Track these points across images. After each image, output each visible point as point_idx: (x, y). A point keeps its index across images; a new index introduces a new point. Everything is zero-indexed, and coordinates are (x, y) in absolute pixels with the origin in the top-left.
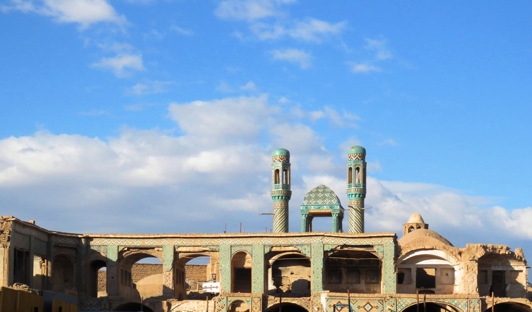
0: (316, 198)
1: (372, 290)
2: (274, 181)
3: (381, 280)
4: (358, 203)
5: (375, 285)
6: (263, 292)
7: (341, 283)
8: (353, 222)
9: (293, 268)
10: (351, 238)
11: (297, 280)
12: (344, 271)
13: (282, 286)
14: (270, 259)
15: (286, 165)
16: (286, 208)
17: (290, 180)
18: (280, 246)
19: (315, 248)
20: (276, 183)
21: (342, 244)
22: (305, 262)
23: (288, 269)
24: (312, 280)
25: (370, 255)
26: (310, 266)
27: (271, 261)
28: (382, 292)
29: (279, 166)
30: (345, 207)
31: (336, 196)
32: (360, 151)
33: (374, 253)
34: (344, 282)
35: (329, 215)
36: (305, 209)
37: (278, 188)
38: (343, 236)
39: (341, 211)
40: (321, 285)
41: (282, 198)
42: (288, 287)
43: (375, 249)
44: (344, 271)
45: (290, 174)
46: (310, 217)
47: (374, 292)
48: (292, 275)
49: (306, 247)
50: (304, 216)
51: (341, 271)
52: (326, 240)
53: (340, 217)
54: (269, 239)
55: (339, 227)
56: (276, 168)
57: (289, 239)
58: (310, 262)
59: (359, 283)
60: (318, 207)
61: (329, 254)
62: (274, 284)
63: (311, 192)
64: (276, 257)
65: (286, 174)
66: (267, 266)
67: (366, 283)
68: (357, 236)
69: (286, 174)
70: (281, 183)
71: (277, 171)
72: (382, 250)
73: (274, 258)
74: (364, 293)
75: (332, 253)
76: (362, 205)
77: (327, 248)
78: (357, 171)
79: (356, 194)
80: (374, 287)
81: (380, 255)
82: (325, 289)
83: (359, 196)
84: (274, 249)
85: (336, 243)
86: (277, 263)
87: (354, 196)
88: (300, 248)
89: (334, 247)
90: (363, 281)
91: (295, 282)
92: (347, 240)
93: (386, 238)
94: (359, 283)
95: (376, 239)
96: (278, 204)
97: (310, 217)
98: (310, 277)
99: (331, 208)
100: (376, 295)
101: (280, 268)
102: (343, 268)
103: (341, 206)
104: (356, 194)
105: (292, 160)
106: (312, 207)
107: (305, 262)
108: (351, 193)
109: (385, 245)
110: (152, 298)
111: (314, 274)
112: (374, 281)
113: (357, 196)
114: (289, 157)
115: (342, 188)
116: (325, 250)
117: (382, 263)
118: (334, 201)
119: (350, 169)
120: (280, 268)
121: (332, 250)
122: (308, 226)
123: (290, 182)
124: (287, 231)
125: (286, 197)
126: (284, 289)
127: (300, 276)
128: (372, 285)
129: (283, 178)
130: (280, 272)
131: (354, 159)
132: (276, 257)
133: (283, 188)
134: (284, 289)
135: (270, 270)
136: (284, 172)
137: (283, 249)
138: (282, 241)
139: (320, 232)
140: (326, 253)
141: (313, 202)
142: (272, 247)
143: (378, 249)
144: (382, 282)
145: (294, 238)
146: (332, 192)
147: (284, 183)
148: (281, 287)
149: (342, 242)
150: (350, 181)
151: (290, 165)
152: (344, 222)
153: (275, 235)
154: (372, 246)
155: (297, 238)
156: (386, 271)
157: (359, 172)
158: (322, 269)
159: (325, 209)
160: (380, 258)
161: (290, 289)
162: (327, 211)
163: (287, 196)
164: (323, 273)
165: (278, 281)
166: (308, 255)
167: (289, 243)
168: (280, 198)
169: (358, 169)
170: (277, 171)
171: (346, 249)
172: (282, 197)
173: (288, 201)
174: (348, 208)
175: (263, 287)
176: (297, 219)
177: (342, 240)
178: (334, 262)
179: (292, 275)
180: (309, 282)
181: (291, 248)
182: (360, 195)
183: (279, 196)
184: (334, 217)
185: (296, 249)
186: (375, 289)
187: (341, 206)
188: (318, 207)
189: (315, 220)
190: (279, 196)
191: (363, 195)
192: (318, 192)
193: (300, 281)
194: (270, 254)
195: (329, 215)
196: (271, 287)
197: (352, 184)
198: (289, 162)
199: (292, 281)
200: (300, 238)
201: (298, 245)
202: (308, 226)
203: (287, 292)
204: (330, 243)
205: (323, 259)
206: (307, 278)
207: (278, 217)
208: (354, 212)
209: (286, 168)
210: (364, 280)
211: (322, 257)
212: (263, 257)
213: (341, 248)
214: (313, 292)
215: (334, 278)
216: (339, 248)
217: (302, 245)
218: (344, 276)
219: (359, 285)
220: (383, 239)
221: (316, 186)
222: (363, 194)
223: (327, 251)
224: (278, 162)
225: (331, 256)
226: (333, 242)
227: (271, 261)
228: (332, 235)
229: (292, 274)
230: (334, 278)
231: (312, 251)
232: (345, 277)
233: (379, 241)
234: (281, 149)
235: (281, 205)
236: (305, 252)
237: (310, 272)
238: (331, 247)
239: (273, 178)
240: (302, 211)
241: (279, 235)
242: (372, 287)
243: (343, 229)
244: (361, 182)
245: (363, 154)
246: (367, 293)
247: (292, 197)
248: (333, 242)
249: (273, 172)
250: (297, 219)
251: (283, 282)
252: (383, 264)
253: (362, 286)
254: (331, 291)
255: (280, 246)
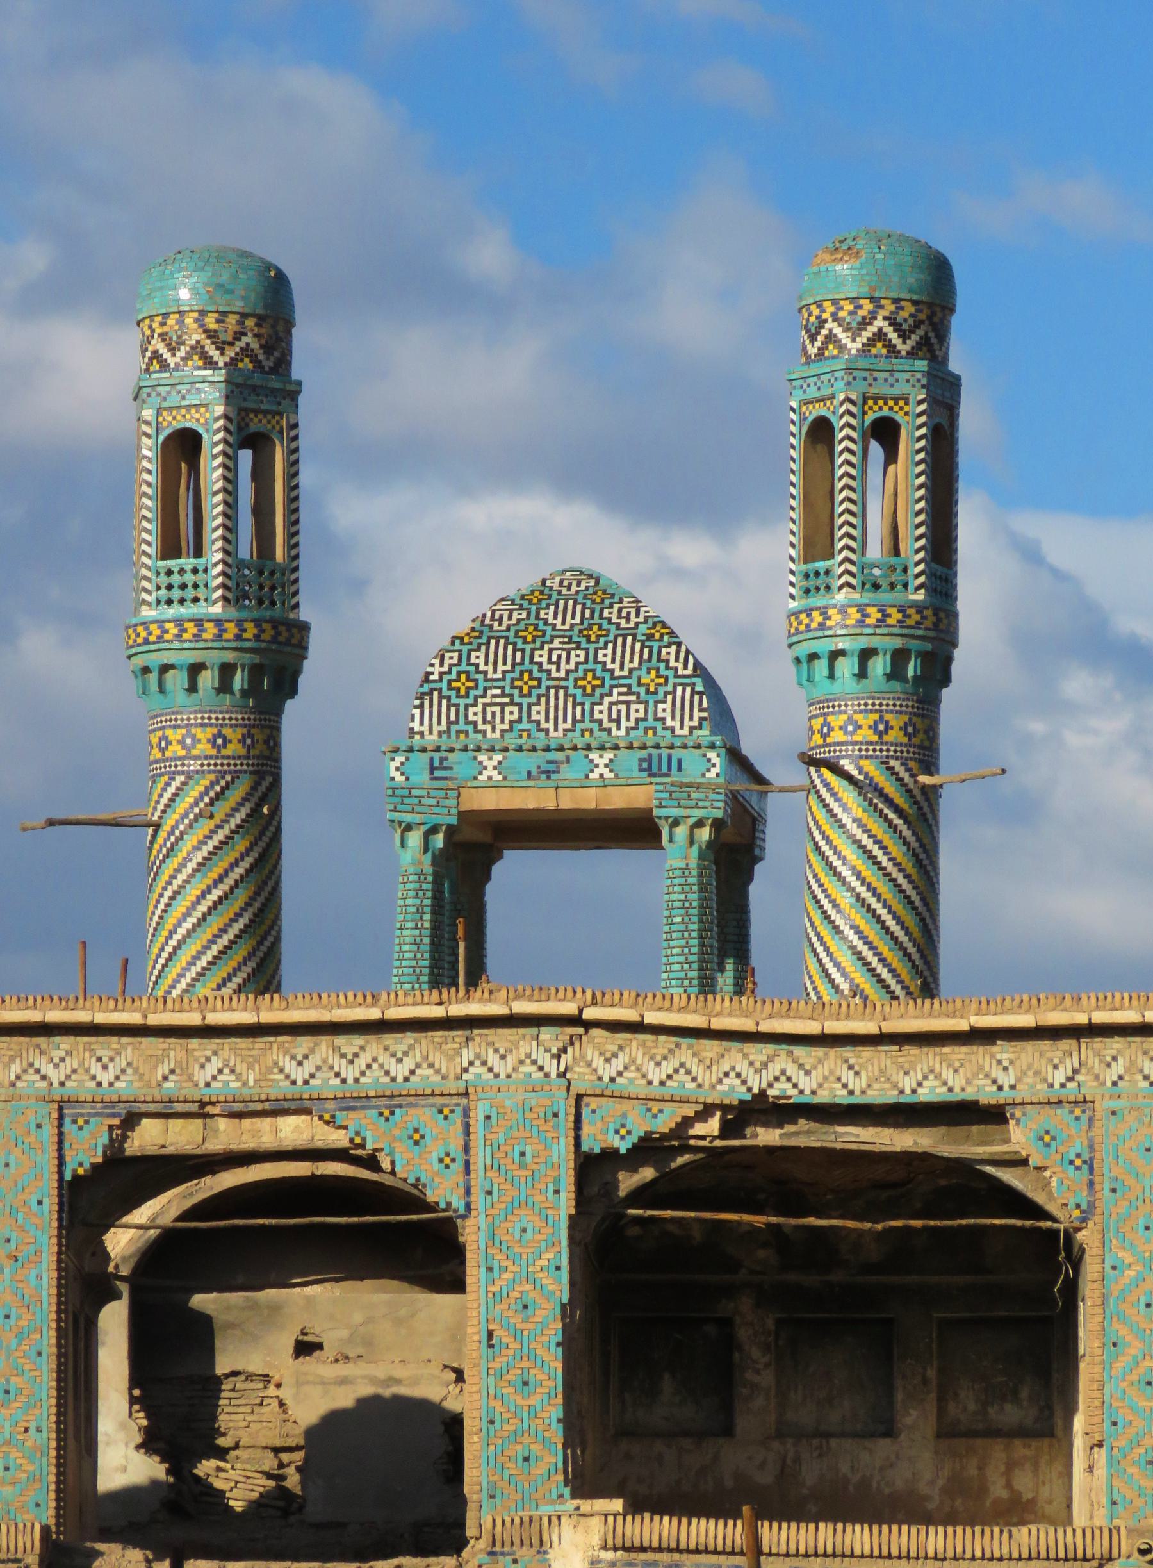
0: (525, 684)
1: (998, 1490)
2: (150, 534)
3: (1070, 1409)
4: (881, 729)
5: (1020, 1449)
6: (48, 1516)
7: (728, 1431)
8: (846, 900)
9: (324, 1303)
10: (820, 1042)
11: (345, 1399)
12: (752, 1326)
13: (221, 1453)
14: (111, 1217)
15: (264, 399)
16: (258, 775)
17: (293, 523)
18: (201, 1111)
19: (498, 1126)
20: (170, 548)
21: (733, 1091)
22: (419, 1247)
23: (275, 1308)
24: (469, 1402)
25: (975, 1189)
26: (458, 1286)
27: (121, 1243)
28: (1080, 1518)
29: (203, 401)
30: (781, 771)
31: (700, 669)
32: (905, 280)
33: (1008, 1176)
34: (754, 1415)
35: (636, 830)
36: (421, 777)
37: (190, 593)
38: (747, 1025)
39: (735, 800)
40: (550, 1455)
41: (224, 686)
42: (269, 1462)
43: (1019, 1137)
44: (752, 1326)
45: (292, 474)
46: (470, 853)
47: (1016, 1511)
48: (302, 1360)
49: (423, 1116)
50: (415, 839)
51: (726, 1323)
52: (598, 1061)
53: (734, 853)
54: (104, 1046)
55: (726, 935)
56: (173, 422)
57: (276, 1050)
58: (458, 1253)
59: (889, 1431)
60: (538, 760)
61: (627, 1182)
62: (150, 1443)
63: (481, 634)
64: (159, 1210)
65: (262, 475)
66: (84, 1287)
67: (948, 1432)
68: (868, 1027)
69: (262, 475)
70: (214, 555)
71: (184, 446)
72: (1079, 1146)
73: (143, 1214)
74: (928, 1520)
75: (648, 1173)
76: (924, 749)
77: (606, 1132)
78: (876, 450)
79: (866, 655)
80: (1011, 1466)
81: (1058, 1193)
82: (584, 1482)
83: (896, 673)
84: (148, 1137)
85: (683, 1084)
86: (175, 1260)
87: (847, 667)
88: (372, 1130)
89: (664, 1122)
90: (917, 1420)
91: (333, 1421)
92: (783, 1060)
93: (1115, 1044)
94: (889, 1431)
95: (1029, 1051)
96: (192, 736)
97: (470, 853)
98: (460, 1376)
99: (649, 768)
100: (1025, 1536)
101: (200, 1301)
102: (746, 1303)
103: (736, 757)
104: (866, 655)
105: (316, 349)
106: (490, 761)
107: (419, 1247)
108: (824, 647)
109: (1103, 1106)
110: (362, 1279)
111: (494, 1350)
112: (1011, 1414)
113: (879, 666)
114: (289, 324)
115: (742, 597)
116: (592, 1142)
117: (1076, 1259)
118: (679, 717)
119: (821, 432)
120: (200, 1301)
121: (648, 1149)
122: (457, 939)
123: (292, 546)
124: (263, 973)
125: (255, 672)
126: (238, 1481)
127: (380, 1371)
128: (998, 1452)
129: (231, 506)
130: (201, 1333)
131: (854, 347)
132: (159, 1210)
133: (235, 594)
134: (238, 1481)
135: (114, 1322)
136: (246, 457)
137: (226, 1136)
138: (216, 1070)
139: (541, 992)
140: (593, 1169)
141: (491, 717)
142: (131, 1121)
143: (1046, 1138)
144: (1079, 1423)
145: (324, 1041)
146: (660, 632)
147: (246, 548)
148: (206, 1467)
149: (739, 1074)
150: (817, 542)
151: (292, 394)
152: (762, 892)
153: (154, 1020)
154: (994, 1115)
155: (350, 1043)
156: (1119, 1331)
157: (891, 456)
158: (567, 1311)
159: (602, 782)
160: (1064, 1215)
161: (293, 1481)
162: (620, 799)
163: (269, 665)
164: (567, 1344)
165: (180, 1409)
166: (443, 1191)
167: (280, 1087)
168: (208, 680)
169: (885, 432)
170: (184, 446)
171: (767, 1136)
172: (227, 671)
173: (278, 712)
174: (796, 775)
175: (47, 1467)
176: (360, 876)
177: (736, 1057)
178: (672, 1247)
179: (308, 1364)
180: (454, 1424)
181: (292, 1131)
182: (899, 657)
183: (195, 669)
184: (681, 852)
185: (338, 1139)
186: (1024, 1482)
187: (736, 757)
188: (538, 760)
189: (515, 874)
190: (195, 669)
191: (927, 658)
192: (541, 635)
193: (369, 1406)
194: (120, 1180)
195: (636, 830)
196: (123, 1461)
197: (835, 564)
198: (282, 364)
199: (308, 1410)
200: (374, 1046)
201: (354, 1102)
202: (457, 939)
203: (258, 1506)
204: (630, 1083)
205: (574, 1222)
206: (432, 1388)
207: (193, 848)
208: (850, 805)
209: (256, 425)
210: (932, 1408)
211: (566, 1203)
212: (50, 1205)
213: (727, 1130)
214: (482, 1515)
215: (667, 1384)
216: (713, 1126)
217: (390, 1101)
218: (759, 1372)
219: (884, 1447)
220: (1090, 1049)
221: (528, 581)
222: (925, 658)
223: (609, 1156)
224: (195, 371)
225: (640, 1196)
226: (655, 1075)
227: (121, 1243)
228: (651, 1018)
229: (305, 1348)
230: (667, 1384)
231: (481, 1156)
232: (767, 1379)
233: (1053, 1066)
234: (215, 257)
235: (219, 741)
236: (418, 1159)
237: (456, 1335)
238: (639, 1123)
239: (149, 506)
240: (400, 795)
241: (192, 1018)
242: (999, 1470)
243: (757, 958)
244: (913, 550)
245: (928, 309)
246: (950, 1519)
247: (313, 673)
248: (656, 1075)
249: (149, 449)
250: (360, 876)
251: (223, 1421)
252: (1090, 1269)
253: (914, 1455)
254: (635, 1507)
255: (201, 1111)
